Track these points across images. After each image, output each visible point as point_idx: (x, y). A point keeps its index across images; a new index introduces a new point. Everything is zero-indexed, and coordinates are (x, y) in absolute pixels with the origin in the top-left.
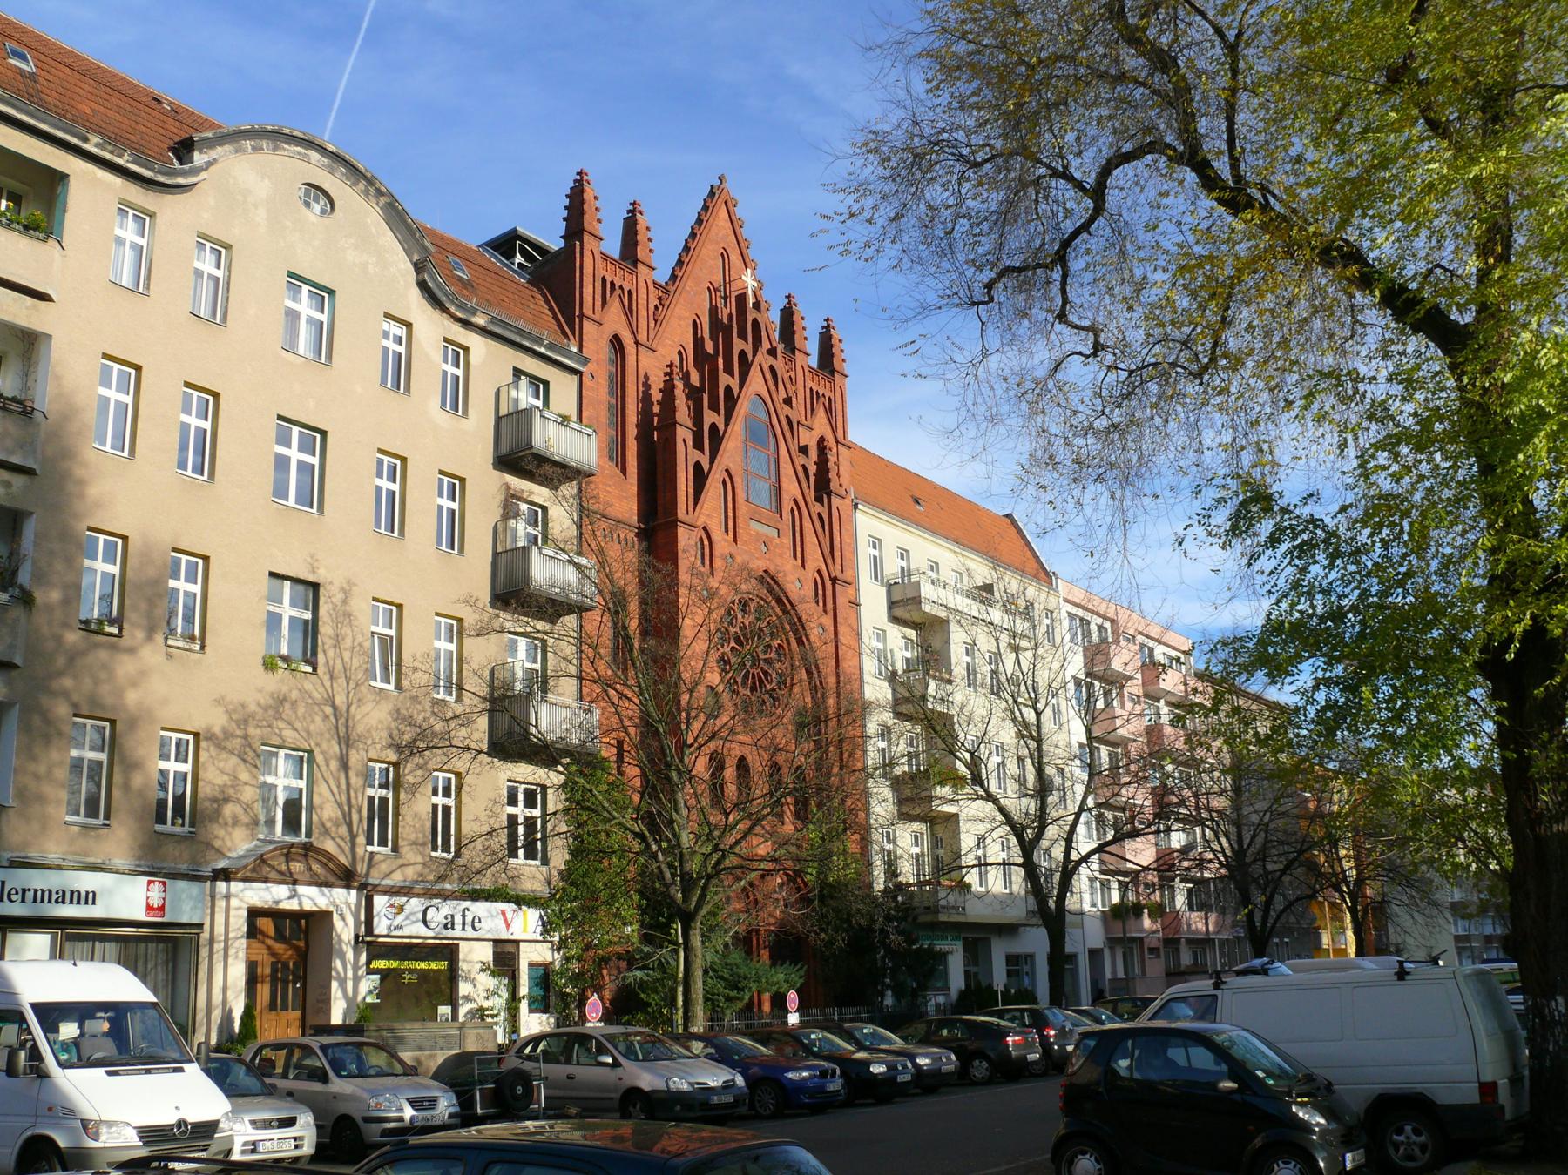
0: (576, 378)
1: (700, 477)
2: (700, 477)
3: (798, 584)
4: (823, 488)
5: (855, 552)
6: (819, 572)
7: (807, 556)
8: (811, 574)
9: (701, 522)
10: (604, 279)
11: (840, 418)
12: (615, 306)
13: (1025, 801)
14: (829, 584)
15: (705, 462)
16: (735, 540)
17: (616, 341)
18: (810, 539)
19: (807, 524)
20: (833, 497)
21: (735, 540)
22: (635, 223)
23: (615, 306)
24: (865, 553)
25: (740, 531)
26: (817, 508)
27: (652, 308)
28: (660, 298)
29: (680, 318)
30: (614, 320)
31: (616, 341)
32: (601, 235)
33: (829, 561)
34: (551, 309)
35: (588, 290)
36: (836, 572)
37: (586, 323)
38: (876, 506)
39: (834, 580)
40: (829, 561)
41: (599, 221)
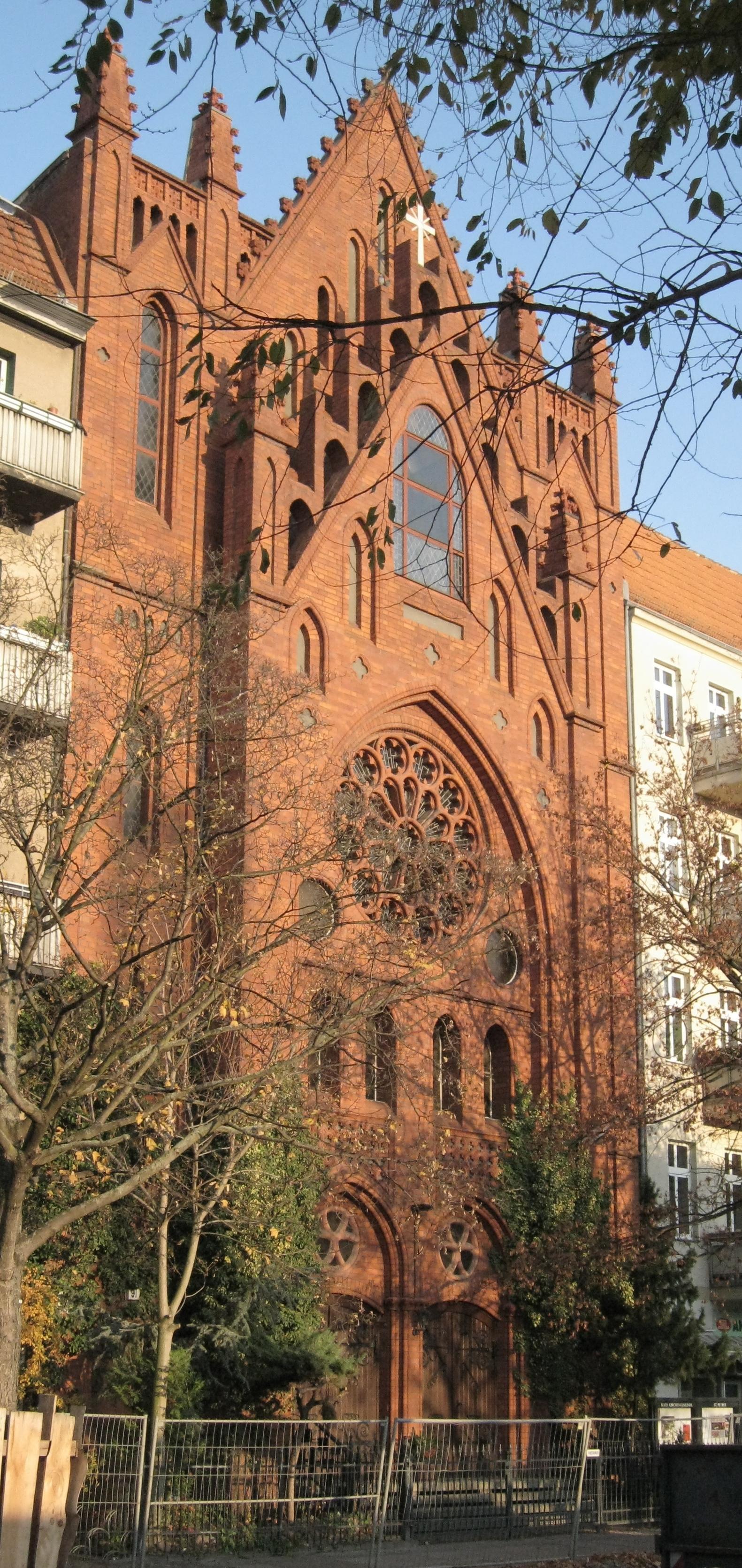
0: (66, 358)
1: (301, 521)
2: (301, 521)
3: (506, 728)
4: (555, 569)
5: (627, 685)
6: (542, 702)
7: (519, 676)
8: (525, 704)
9: (304, 595)
10: (138, 204)
11: (604, 469)
12: (158, 241)
13: (675, 839)
14: (561, 724)
15: (314, 500)
16: (373, 638)
17: (160, 305)
18: (525, 642)
19: (521, 623)
20: (573, 584)
21: (373, 638)
22: (209, 122)
23: (158, 241)
24: (645, 694)
25: (383, 622)
26: (543, 598)
27: (235, 257)
28: (252, 244)
29: (292, 280)
30: (157, 266)
31: (160, 305)
32: (240, 188)
33: (563, 687)
34: (44, 250)
35: (104, 216)
36: (577, 703)
37: (96, 268)
38: (658, 611)
39: (570, 718)
40: (563, 687)
41: (237, 167)
